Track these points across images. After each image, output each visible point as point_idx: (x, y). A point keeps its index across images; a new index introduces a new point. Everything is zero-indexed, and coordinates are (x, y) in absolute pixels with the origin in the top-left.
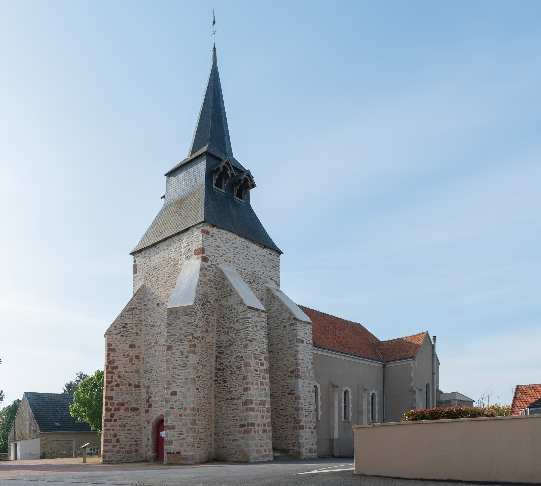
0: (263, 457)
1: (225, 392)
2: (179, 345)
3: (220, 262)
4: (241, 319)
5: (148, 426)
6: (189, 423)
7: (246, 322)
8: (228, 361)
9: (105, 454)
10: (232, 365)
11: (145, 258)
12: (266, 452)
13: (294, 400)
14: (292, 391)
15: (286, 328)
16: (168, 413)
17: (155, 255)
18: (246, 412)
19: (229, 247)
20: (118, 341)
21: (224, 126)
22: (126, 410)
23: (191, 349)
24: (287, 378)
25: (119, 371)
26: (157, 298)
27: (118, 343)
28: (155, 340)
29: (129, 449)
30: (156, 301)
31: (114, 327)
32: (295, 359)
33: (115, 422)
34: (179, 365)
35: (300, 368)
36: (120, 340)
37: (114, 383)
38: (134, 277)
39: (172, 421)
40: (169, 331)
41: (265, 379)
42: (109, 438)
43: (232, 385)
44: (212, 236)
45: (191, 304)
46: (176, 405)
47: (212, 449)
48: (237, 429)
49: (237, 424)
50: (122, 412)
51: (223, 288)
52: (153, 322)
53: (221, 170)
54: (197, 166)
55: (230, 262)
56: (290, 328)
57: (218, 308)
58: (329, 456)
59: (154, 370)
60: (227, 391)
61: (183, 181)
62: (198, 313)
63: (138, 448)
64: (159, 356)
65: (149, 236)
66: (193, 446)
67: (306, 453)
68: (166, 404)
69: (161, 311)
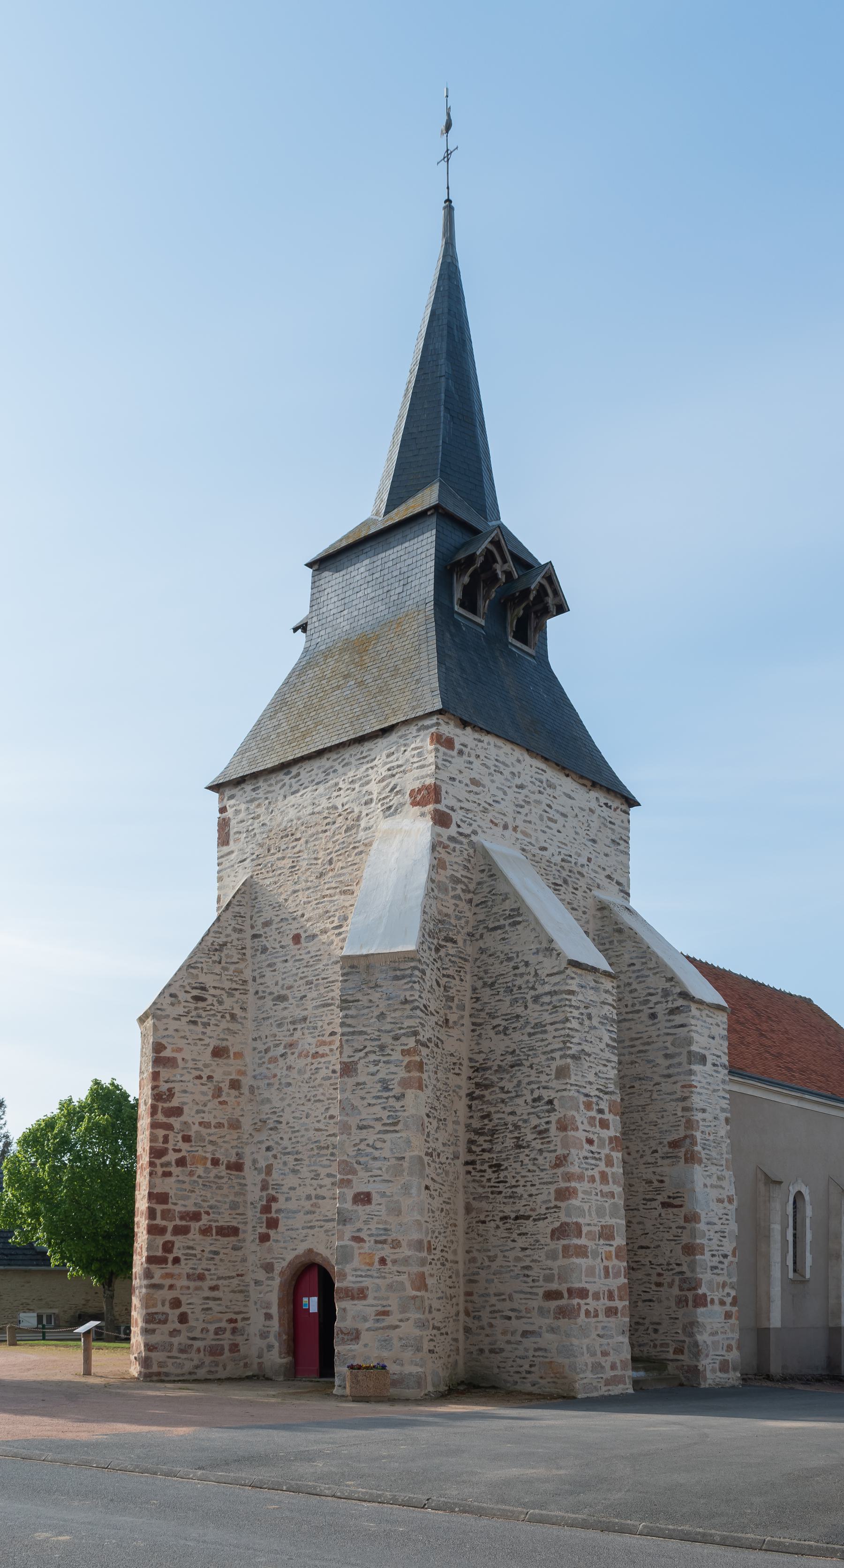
0: (608, 1383)
1: (500, 1198)
2: (376, 1063)
3: (479, 826)
4: (546, 994)
5: (268, 1279)
6: (408, 1285)
7: (563, 1003)
8: (508, 1109)
9: (150, 1354)
10: (520, 1123)
11: (257, 803)
12: (616, 1369)
13: (681, 1222)
14: (674, 1198)
15: (656, 1021)
16: (345, 1255)
17: (285, 797)
18: (564, 1257)
19: (503, 784)
20: (182, 1037)
21: (479, 431)
22: (205, 1231)
23: (411, 1074)
24: (660, 1162)
25: (185, 1123)
26: (294, 919)
27: (182, 1043)
28: (288, 1040)
29: (214, 1343)
30: (293, 928)
31: (172, 995)
32: (685, 1109)
33: (176, 1265)
34: (377, 1119)
35: (698, 1135)
36: (188, 1034)
37: (172, 1157)
38: (222, 854)
39: (357, 1276)
40: (349, 1021)
41: (612, 1166)
42: (159, 1309)
43: (518, 1177)
44: (461, 753)
45: (411, 947)
46: (369, 1232)
47: (458, 1354)
48: (535, 1304)
49: (535, 1290)
50: (194, 1237)
51: (490, 903)
52: (282, 987)
53: (479, 561)
54: (406, 544)
55: (505, 827)
56: (670, 1021)
57: (476, 959)
58: (755, 1375)
59: (284, 1123)
60: (503, 1194)
61: (362, 587)
62: (428, 972)
63: (239, 1339)
64: (300, 1084)
65: (264, 740)
66: (419, 1349)
67: (713, 1371)
68: (340, 1227)
69: (306, 957)
